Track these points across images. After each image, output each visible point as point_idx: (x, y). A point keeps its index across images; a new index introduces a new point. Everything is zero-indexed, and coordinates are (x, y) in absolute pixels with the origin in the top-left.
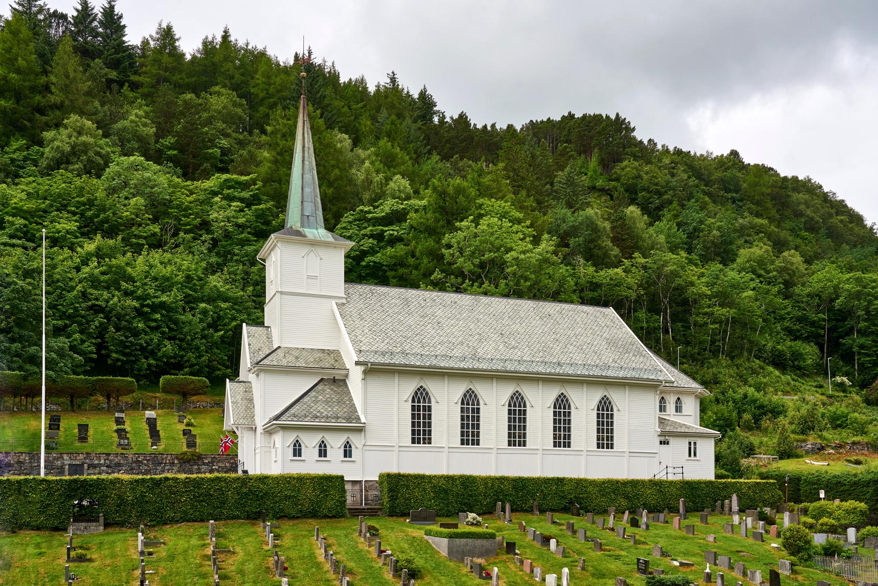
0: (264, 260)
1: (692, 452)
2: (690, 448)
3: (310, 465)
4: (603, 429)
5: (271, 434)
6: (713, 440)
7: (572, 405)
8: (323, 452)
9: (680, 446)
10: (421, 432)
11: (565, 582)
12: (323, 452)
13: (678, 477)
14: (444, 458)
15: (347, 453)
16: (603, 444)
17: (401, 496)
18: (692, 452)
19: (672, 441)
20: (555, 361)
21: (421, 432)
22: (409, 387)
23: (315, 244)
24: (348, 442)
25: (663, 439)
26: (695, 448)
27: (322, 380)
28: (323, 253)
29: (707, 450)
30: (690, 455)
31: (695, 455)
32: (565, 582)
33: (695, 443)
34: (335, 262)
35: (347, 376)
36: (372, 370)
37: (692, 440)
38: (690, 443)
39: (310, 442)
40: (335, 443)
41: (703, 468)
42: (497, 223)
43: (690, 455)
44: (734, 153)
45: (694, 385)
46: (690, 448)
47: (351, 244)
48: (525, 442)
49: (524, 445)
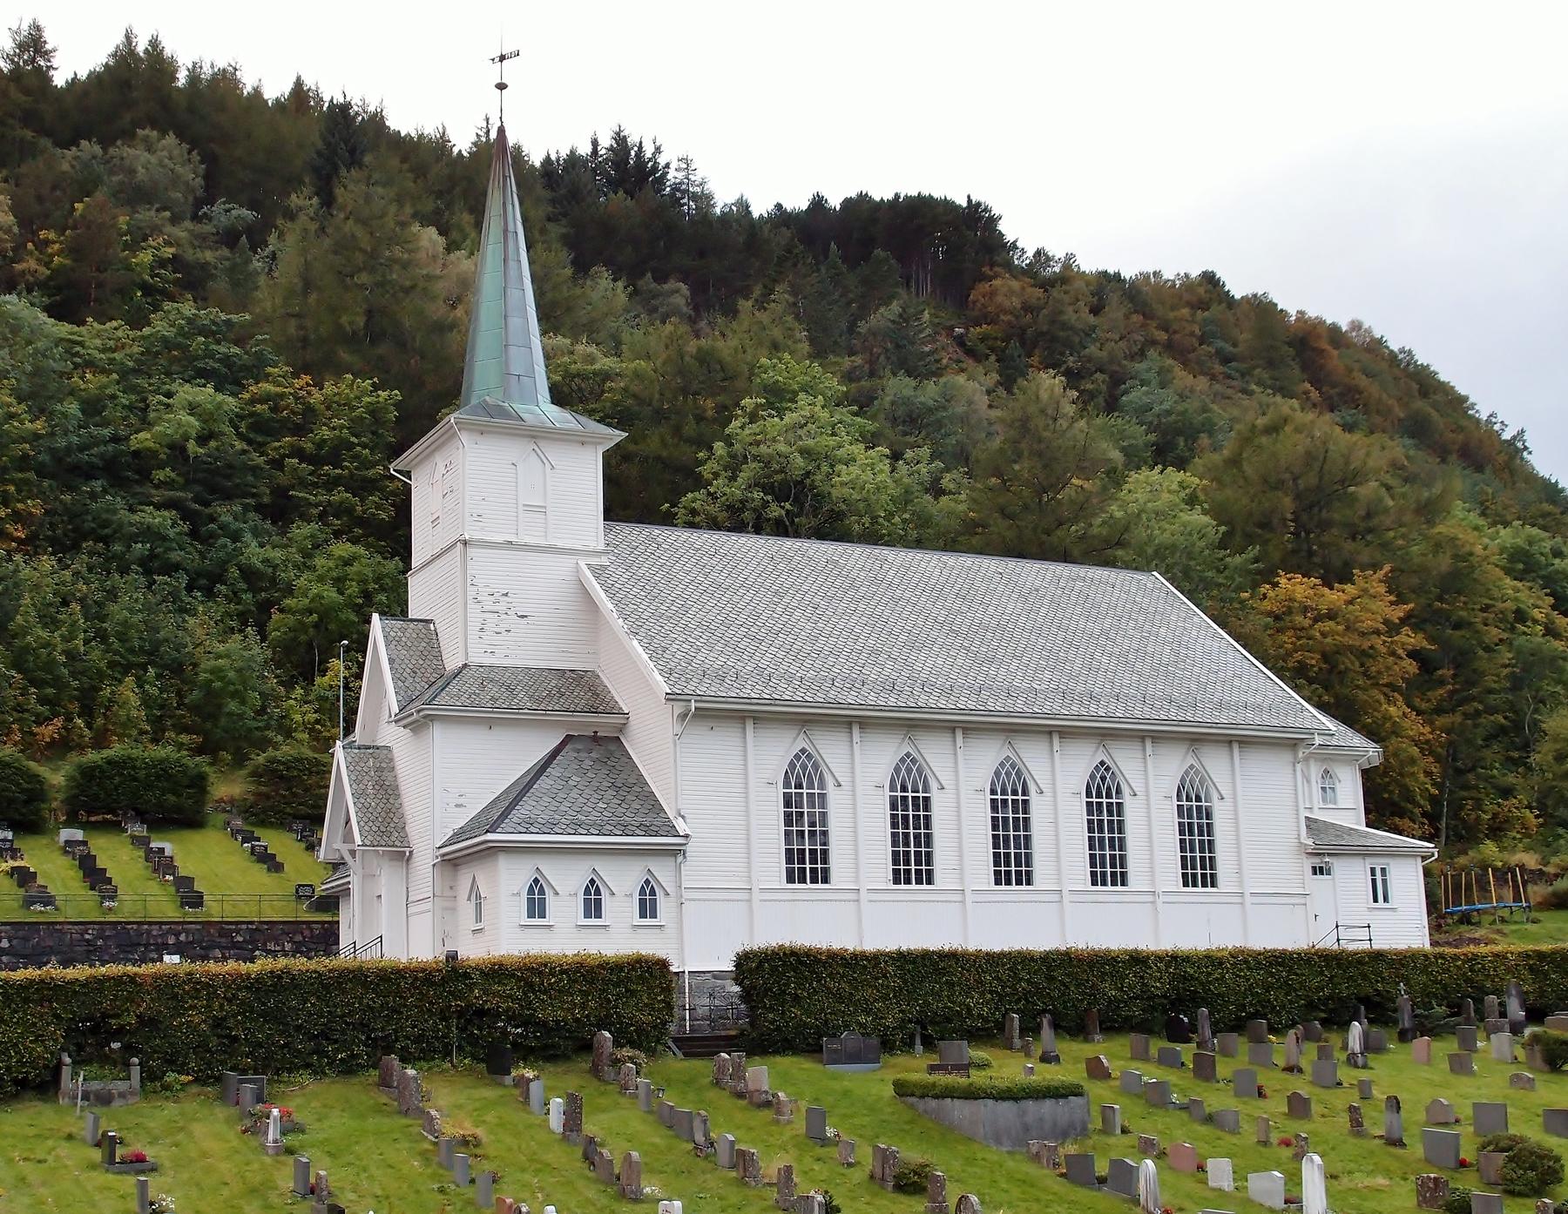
0: (408, 475)
1: (1379, 892)
2: (1374, 882)
3: (565, 938)
4: (1101, 840)
5: (456, 865)
6: (1420, 865)
7: (1124, 788)
8: (593, 907)
9: (1352, 876)
10: (808, 862)
11: (3, 974)
12: (593, 907)
13: (1366, 946)
14: (860, 914)
15: (647, 908)
16: (1008, 873)
17: (792, 1002)
18: (1379, 892)
19: (1338, 865)
20: (1080, 688)
21: (808, 862)
22: (772, 754)
23: (538, 435)
24: (536, 881)
25: (1316, 861)
26: (1384, 882)
27: (568, 739)
28: (554, 453)
29: (1408, 883)
30: (1376, 900)
31: (1386, 900)
32: (3, 974)
33: (1383, 870)
34: (578, 476)
35: (622, 728)
36: (708, 715)
37: (1378, 863)
38: (1373, 871)
39: (566, 880)
40: (623, 881)
41: (1401, 924)
42: (806, 416)
43: (1376, 900)
44: (1210, 279)
45: (1356, 740)
46: (1374, 882)
47: (618, 436)
48: (826, 872)
49: (826, 880)
